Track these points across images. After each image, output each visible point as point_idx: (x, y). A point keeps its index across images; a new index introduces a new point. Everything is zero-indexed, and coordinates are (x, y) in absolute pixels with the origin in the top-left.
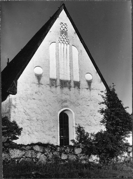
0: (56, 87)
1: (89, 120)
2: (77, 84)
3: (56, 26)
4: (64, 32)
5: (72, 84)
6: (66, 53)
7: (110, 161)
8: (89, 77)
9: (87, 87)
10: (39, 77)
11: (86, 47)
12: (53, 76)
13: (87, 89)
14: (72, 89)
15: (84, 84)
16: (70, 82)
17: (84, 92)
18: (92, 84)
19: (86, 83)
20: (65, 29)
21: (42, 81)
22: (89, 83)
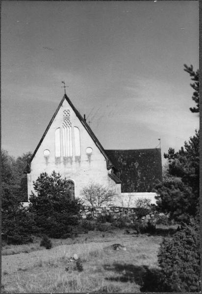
0: (60, 163)
1: (56, 284)
2: (78, 159)
3: (61, 110)
4: (67, 118)
5: (74, 159)
6: (70, 146)
7: (164, 281)
8: (89, 151)
9: (87, 159)
10: (47, 158)
11: (84, 126)
12: (58, 155)
13: (87, 161)
14: (74, 163)
15: (84, 158)
16: (71, 158)
17: (85, 165)
18: (92, 156)
19: (86, 156)
20: (68, 115)
21: (49, 160)
22: (89, 155)
